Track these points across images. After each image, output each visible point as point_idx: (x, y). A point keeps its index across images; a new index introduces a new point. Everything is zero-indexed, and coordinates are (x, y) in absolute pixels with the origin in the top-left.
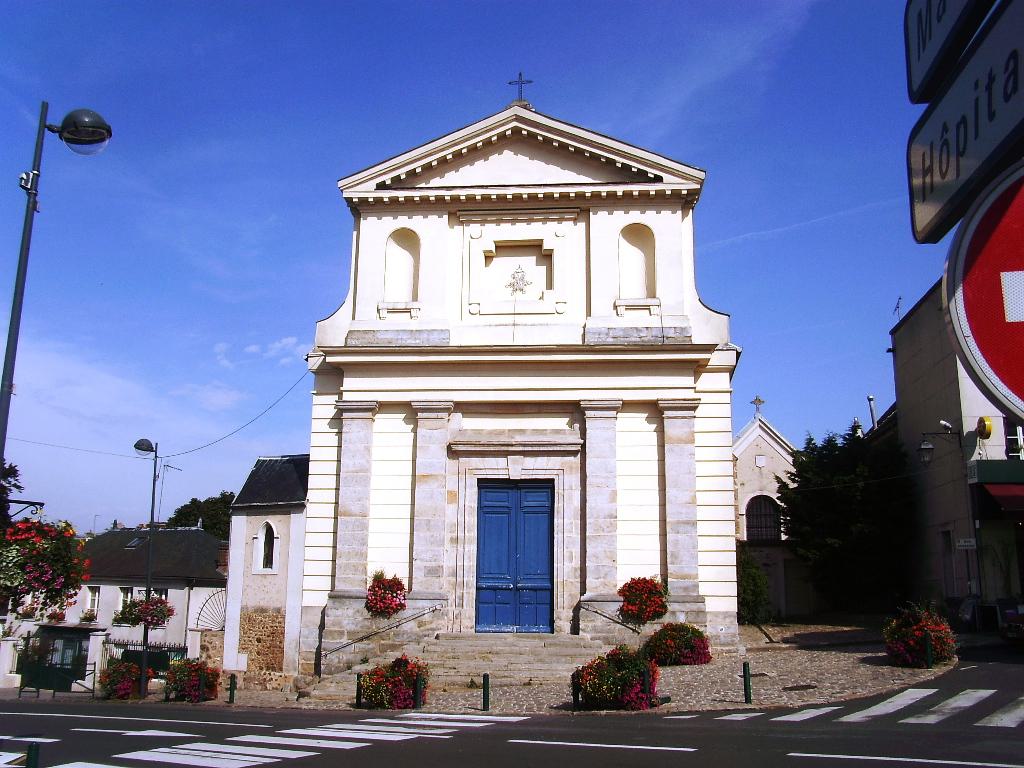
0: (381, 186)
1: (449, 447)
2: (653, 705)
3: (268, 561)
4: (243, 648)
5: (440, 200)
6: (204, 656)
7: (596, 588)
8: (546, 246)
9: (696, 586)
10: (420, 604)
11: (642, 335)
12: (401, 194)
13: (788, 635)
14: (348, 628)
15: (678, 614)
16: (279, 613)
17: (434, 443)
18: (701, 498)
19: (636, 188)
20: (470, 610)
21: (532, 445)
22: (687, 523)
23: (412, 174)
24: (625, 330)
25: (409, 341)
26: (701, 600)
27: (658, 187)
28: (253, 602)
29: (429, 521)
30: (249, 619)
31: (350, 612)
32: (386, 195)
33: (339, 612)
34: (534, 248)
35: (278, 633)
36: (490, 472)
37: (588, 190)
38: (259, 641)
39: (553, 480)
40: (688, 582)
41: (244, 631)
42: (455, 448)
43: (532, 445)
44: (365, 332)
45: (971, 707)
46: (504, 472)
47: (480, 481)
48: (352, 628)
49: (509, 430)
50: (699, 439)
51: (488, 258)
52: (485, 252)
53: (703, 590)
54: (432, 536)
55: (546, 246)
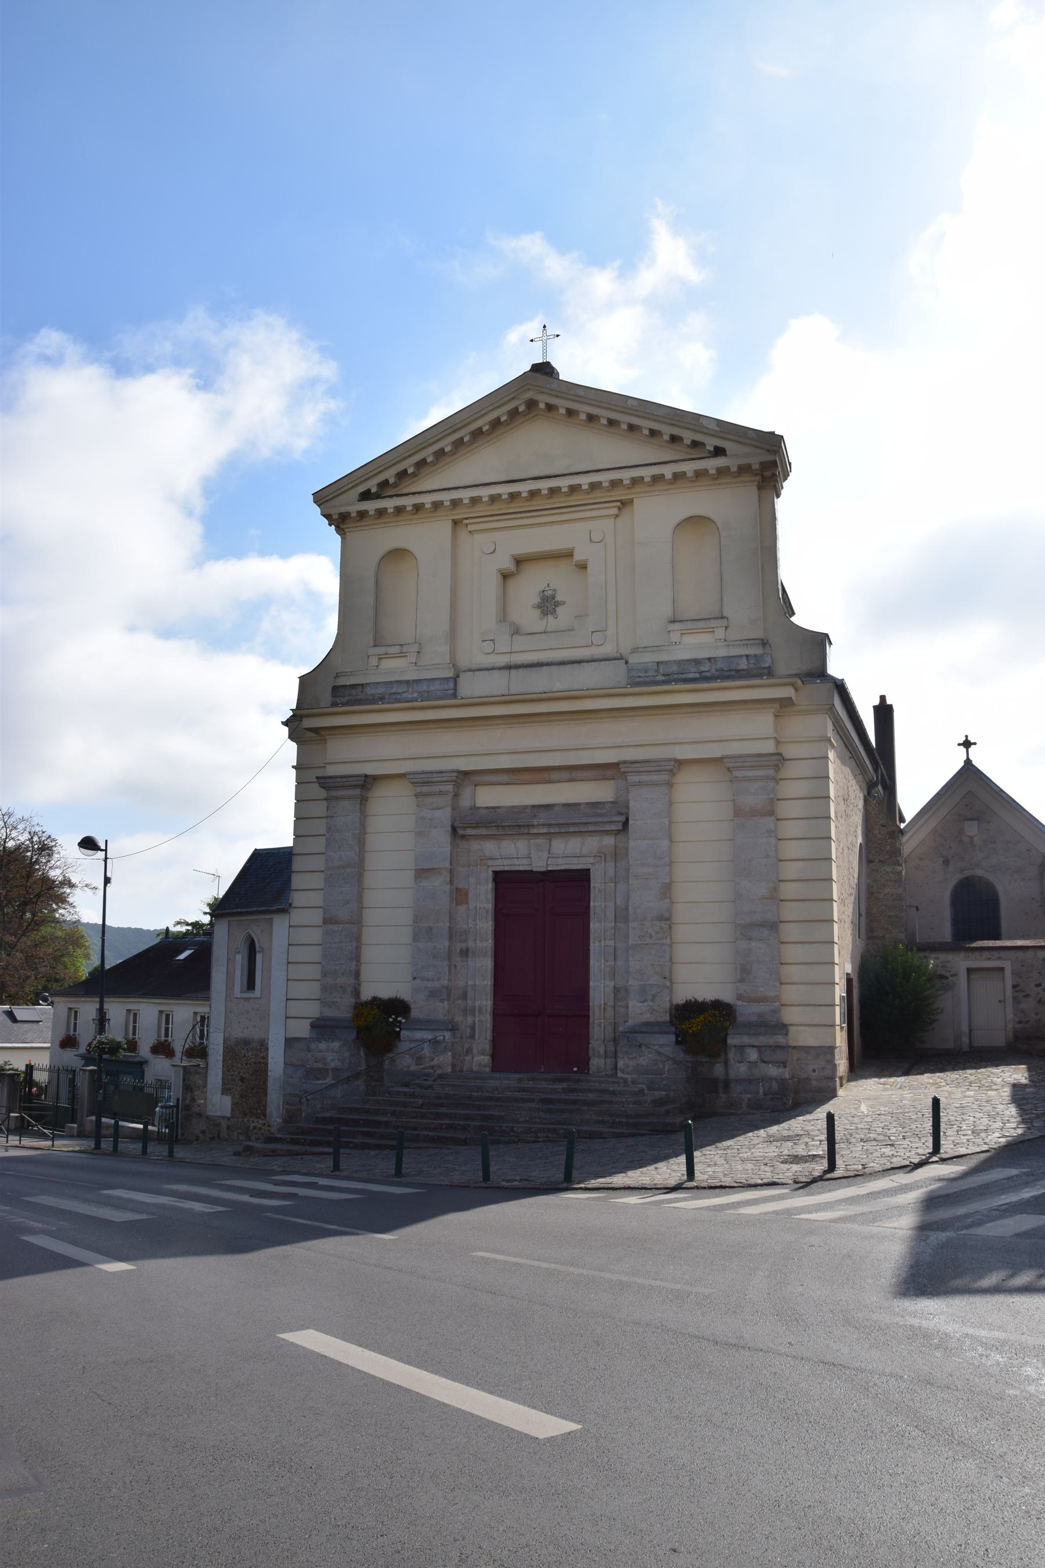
0: (366, 496)
1: (454, 829)
2: (644, 1096)
3: (251, 985)
4: (225, 1091)
5: (437, 505)
6: (188, 1097)
7: (641, 1014)
8: (578, 557)
9: (776, 1012)
10: (419, 1035)
11: (703, 668)
12: (389, 504)
13: (690, 1060)
14: (333, 1065)
15: (749, 1050)
16: (263, 1046)
17: (435, 827)
18: (789, 890)
19: (689, 468)
20: (483, 1040)
21: (493, 521)
22: (763, 924)
23: (403, 475)
24: (680, 663)
25: (404, 695)
26: (783, 1028)
27: (720, 462)
28: (238, 1032)
29: (431, 928)
30: (233, 1051)
31: (336, 1045)
32: (371, 506)
33: (323, 1046)
34: (567, 555)
35: (261, 1070)
36: (506, 862)
37: (647, 473)
38: (242, 1079)
39: (588, 870)
40: (762, 1008)
41: (227, 1069)
42: (461, 832)
43: (493, 521)
44: (353, 686)
45: (92, 924)
46: (525, 861)
47: (495, 873)
48: (337, 1064)
49: (533, 806)
50: (786, 809)
51: (506, 576)
52: (499, 570)
53: (790, 1016)
54: (435, 948)
55: (578, 557)
